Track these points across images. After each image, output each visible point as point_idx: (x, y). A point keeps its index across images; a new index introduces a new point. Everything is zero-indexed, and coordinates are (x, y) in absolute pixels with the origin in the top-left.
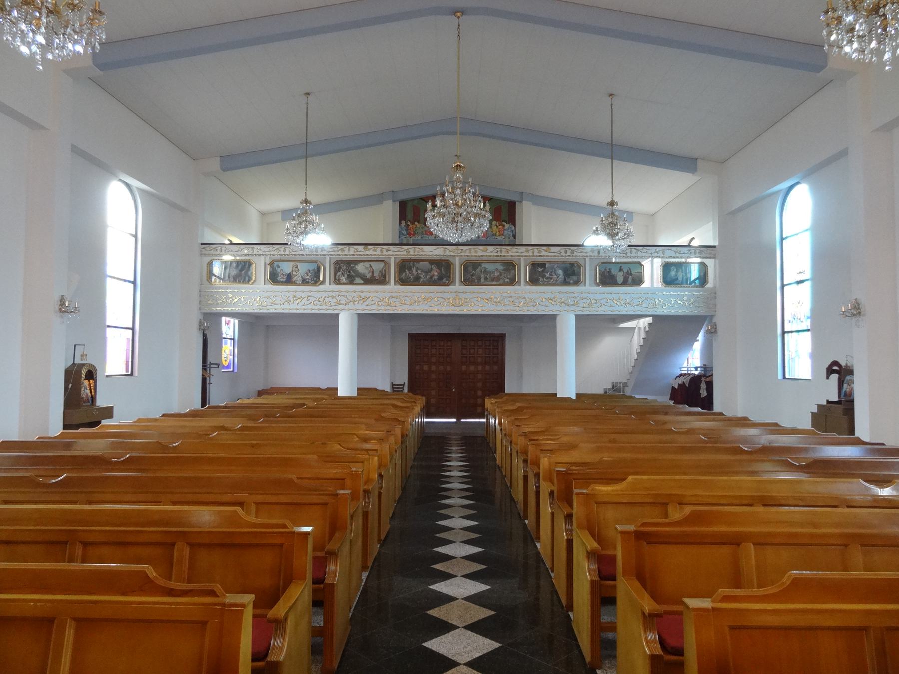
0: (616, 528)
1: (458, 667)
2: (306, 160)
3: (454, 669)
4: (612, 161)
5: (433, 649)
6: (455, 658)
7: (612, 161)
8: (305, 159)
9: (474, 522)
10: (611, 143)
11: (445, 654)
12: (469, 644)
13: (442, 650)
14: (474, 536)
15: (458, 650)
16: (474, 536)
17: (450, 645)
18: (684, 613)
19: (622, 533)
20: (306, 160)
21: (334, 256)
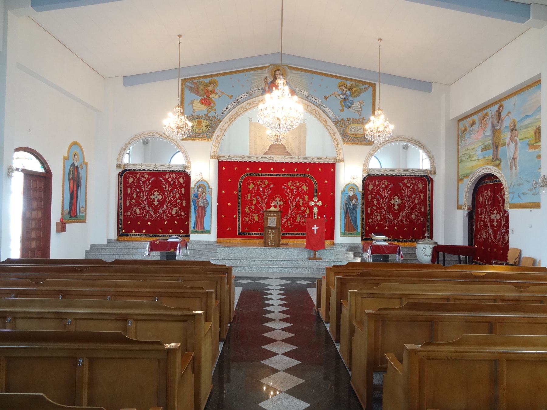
0: (365, 312)
1: (286, 390)
2: (179, 67)
3: (288, 389)
4: (281, 52)
5: (302, 402)
6: (288, 395)
7: (281, 52)
8: (178, 79)
9: (268, 288)
10: (280, 52)
11: (294, 398)
12: (280, 405)
13: (297, 401)
14: (282, 297)
15: (286, 401)
16: (282, 297)
17: (292, 404)
18: (371, 122)
19: (367, 314)
20: (179, 67)
21: (114, 254)
